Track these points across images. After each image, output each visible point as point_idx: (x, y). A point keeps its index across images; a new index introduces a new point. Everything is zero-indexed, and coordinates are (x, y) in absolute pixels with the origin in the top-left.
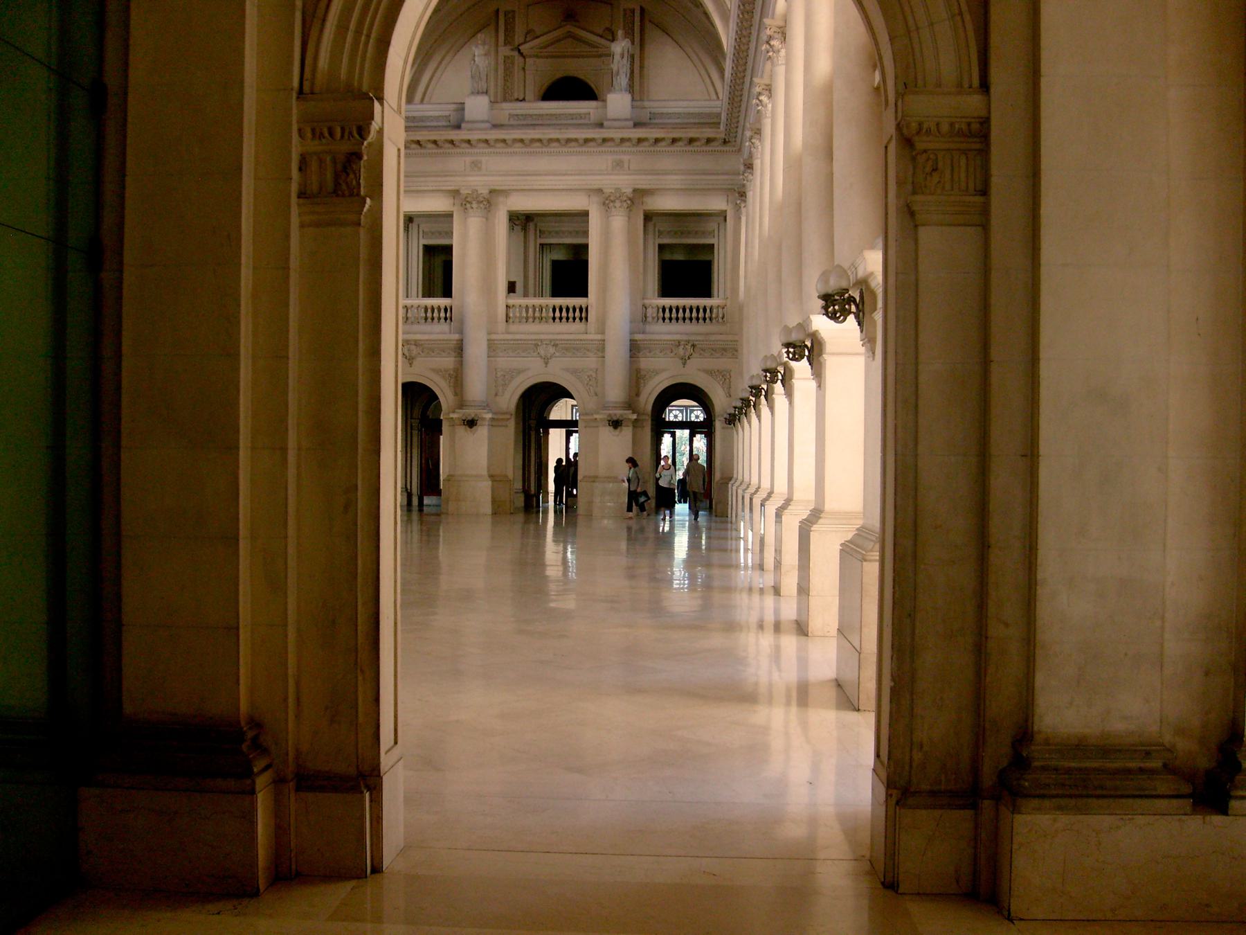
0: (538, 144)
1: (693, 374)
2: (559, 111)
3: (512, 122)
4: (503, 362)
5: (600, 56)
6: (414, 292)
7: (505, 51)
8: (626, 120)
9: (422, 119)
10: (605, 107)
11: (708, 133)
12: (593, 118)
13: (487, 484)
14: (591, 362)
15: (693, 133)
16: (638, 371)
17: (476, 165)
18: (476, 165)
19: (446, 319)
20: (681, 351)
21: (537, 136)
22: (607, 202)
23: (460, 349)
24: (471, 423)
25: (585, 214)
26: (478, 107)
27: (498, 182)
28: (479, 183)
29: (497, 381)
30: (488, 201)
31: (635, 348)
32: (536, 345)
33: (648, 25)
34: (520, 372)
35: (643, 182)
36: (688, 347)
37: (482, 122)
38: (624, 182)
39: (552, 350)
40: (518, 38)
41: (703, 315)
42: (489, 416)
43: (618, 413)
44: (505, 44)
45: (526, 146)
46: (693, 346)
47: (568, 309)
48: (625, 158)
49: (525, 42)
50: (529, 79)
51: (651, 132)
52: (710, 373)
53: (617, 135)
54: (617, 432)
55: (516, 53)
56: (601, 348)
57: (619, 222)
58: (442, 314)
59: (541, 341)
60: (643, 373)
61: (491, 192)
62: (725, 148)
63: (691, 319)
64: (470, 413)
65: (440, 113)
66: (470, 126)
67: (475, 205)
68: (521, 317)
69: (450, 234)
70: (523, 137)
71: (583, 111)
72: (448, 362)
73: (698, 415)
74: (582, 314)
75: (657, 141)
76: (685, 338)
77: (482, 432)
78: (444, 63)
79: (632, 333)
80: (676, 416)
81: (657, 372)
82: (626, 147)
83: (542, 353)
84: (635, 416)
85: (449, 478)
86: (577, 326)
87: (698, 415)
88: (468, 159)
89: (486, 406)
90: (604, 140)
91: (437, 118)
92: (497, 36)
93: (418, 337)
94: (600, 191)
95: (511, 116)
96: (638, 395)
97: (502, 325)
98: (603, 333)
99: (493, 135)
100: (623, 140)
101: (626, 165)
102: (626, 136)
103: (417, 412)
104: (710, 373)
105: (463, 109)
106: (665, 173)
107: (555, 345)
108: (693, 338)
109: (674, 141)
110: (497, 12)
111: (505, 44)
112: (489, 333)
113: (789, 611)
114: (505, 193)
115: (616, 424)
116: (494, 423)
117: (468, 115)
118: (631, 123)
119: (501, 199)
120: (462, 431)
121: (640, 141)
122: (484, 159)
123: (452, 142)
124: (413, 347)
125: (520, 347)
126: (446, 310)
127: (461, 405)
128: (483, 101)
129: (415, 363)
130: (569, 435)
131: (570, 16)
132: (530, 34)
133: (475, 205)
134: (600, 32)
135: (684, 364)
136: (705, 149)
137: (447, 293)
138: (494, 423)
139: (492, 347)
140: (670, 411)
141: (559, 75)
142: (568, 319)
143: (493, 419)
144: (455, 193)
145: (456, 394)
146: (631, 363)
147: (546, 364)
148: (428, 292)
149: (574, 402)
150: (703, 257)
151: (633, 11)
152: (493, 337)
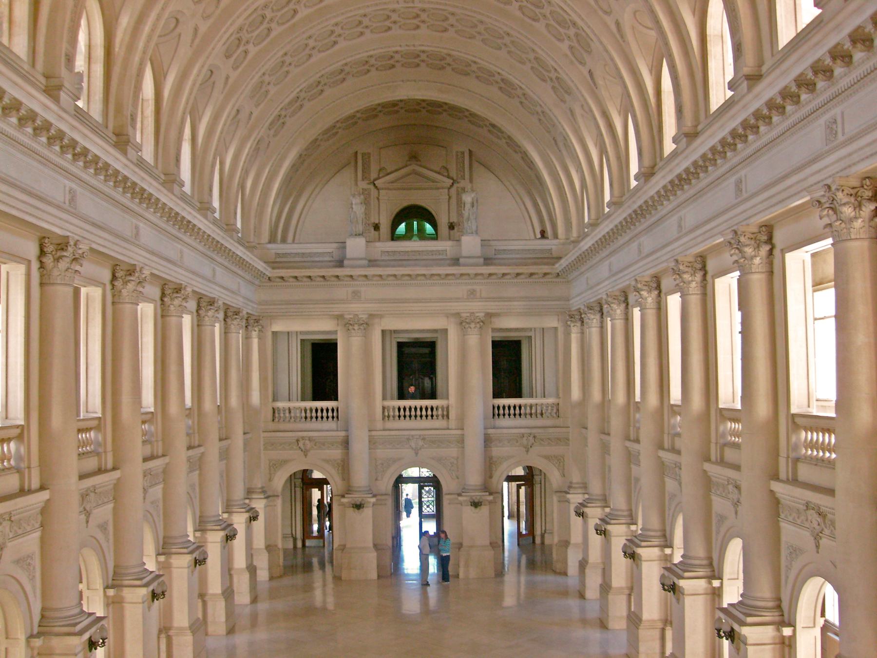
0: (407, 278)
2: (421, 249)
3: (384, 258)
4: (382, 453)
5: (438, 188)
7: (363, 185)
8: (478, 257)
10: (460, 246)
12: (450, 254)
13: (373, 556)
16: (491, 458)
19: (333, 417)
20: (524, 441)
22: (463, 324)
23: (346, 443)
24: (358, 507)
28: (359, 309)
31: (488, 441)
32: (408, 439)
33: (475, 165)
35: (492, 307)
36: (531, 438)
37: (361, 259)
38: (478, 307)
39: (421, 443)
40: (374, 175)
43: (477, 495)
44: (363, 180)
46: (534, 437)
48: (477, 288)
49: (379, 178)
50: (383, 207)
52: (547, 458)
54: (477, 510)
55: (371, 187)
56: (461, 441)
57: (473, 340)
58: (330, 414)
59: (413, 436)
60: (494, 459)
62: (557, 280)
63: (531, 414)
64: (357, 497)
66: (351, 262)
67: (356, 327)
68: (394, 417)
70: (396, 273)
71: (440, 248)
78: (317, 190)
83: (413, 445)
84: (491, 498)
85: (343, 548)
88: (350, 290)
92: (356, 171)
94: (458, 314)
95: (383, 252)
96: (491, 477)
97: (379, 424)
101: (478, 295)
104: (547, 458)
105: (345, 248)
106: (510, 299)
107: (424, 439)
108: (534, 431)
110: (356, 153)
111: (363, 180)
113: (593, 611)
114: (381, 317)
115: (476, 504)
117: (349, 253)
119: (377, 321)
120: (351, 512)
124: (307, 442)
126: (333, 410)
127: (348, 490)
128: (361, 241)
129: (309, 454)
131: (414, 157)
132: (383, 172)
134: (438, 169)
135: (527, 451)
136: (541, 280)
137: (333, 395)
139: (373, 443)
141: (405, 204)
144: (339, 317)
145: (344, 479)
146: (485, 451)
148: (317, 395)
151: (463, 153)
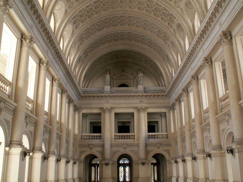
1: (128, 151)
4: (114, 149)
6: (88, 131)
9: (86, 91)
11: (163, 94)
14: (135, 149)
15: (159, 94)
17: (107, 102)
18: (107, 102)
21: (118, 95)
24: (107, 164)
25: (83, 114)
26: (107, 88)
27: (112, 106)
29: (113, 153)
30: (110, 110)
31: (146, 145)
34: (154, 150)
39: (126, 146)
41: (129, 137)
42: (112, 162)
43: (143, 161)
45: (111, 97)
47: (96, 136)
48: (143, 100)
51: (147, 94)
52: (165, 150)
53: (141, 94)
56: (138, 145)
61: (111, 108)
64: (107, 162)
65: (98, 90)
69: (101, 119)
72: (100, 149)
73: (127, 162)
74: (100, 137)
75: (150, 96)
76: (159, 142)
77: (110, 166)
79: (146, 141)
80: (126, 162)
81: (152, 151)
82: (143, 97)
86: (132, 140)
87: (127, 162)
88: (106, 100)
89: (110, 160)
90: (138, 96)
91: (97, 91)
93: (93, 143)
94: (137, 108)
97: (113, 140)
98: (139, 142)
99: (112, 95)
100: (142, 96)
101: (143, 102)
102: (143, 95)
103: (88, 162)
104: (165, 150)
108: (160, 142)
109: (154, 96)
112: (111, 142)
116: (112, 164)
118: (110, 92)
121: (146, 96)
122: (109, 100)
123: (102, 96)
124: (92, 145)
125: (118, 145)
130: (154, 166)
133: (107, 111)
136: (161, 98)
138: (112, 164)
139: (111, 145)
140: (128, 161)
142: (95, 138)
143: (112, 163)
147: (125, 149)
149: (98, 159)
150: (127, 125)
152: (112, 143)
